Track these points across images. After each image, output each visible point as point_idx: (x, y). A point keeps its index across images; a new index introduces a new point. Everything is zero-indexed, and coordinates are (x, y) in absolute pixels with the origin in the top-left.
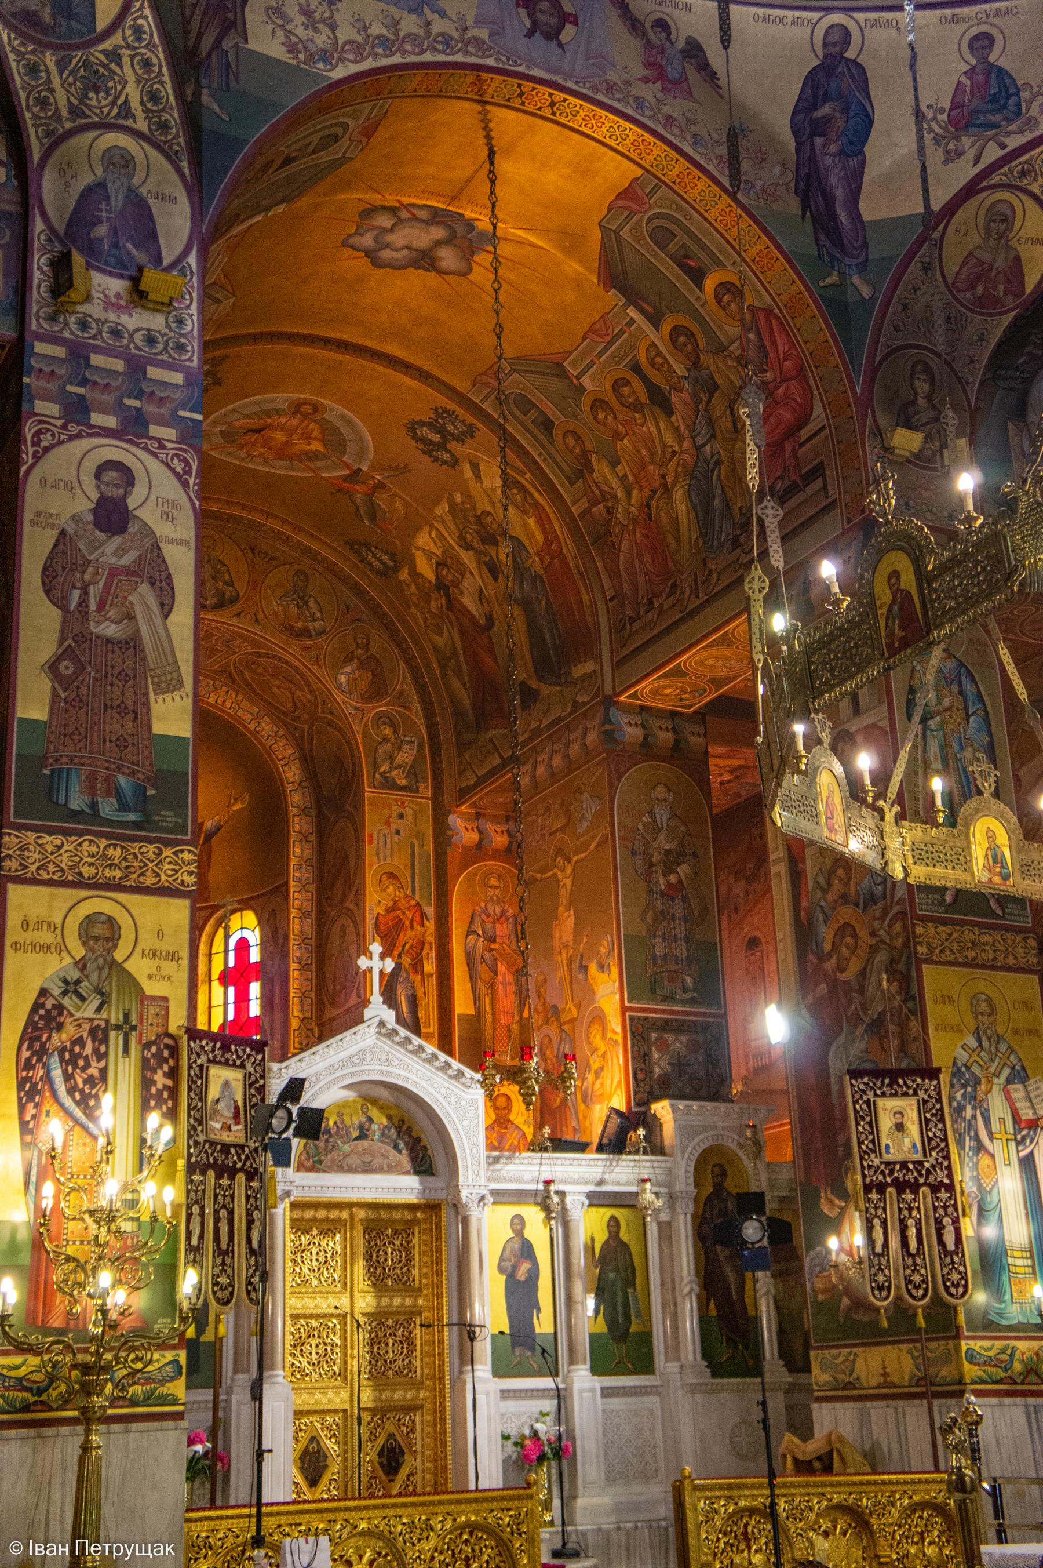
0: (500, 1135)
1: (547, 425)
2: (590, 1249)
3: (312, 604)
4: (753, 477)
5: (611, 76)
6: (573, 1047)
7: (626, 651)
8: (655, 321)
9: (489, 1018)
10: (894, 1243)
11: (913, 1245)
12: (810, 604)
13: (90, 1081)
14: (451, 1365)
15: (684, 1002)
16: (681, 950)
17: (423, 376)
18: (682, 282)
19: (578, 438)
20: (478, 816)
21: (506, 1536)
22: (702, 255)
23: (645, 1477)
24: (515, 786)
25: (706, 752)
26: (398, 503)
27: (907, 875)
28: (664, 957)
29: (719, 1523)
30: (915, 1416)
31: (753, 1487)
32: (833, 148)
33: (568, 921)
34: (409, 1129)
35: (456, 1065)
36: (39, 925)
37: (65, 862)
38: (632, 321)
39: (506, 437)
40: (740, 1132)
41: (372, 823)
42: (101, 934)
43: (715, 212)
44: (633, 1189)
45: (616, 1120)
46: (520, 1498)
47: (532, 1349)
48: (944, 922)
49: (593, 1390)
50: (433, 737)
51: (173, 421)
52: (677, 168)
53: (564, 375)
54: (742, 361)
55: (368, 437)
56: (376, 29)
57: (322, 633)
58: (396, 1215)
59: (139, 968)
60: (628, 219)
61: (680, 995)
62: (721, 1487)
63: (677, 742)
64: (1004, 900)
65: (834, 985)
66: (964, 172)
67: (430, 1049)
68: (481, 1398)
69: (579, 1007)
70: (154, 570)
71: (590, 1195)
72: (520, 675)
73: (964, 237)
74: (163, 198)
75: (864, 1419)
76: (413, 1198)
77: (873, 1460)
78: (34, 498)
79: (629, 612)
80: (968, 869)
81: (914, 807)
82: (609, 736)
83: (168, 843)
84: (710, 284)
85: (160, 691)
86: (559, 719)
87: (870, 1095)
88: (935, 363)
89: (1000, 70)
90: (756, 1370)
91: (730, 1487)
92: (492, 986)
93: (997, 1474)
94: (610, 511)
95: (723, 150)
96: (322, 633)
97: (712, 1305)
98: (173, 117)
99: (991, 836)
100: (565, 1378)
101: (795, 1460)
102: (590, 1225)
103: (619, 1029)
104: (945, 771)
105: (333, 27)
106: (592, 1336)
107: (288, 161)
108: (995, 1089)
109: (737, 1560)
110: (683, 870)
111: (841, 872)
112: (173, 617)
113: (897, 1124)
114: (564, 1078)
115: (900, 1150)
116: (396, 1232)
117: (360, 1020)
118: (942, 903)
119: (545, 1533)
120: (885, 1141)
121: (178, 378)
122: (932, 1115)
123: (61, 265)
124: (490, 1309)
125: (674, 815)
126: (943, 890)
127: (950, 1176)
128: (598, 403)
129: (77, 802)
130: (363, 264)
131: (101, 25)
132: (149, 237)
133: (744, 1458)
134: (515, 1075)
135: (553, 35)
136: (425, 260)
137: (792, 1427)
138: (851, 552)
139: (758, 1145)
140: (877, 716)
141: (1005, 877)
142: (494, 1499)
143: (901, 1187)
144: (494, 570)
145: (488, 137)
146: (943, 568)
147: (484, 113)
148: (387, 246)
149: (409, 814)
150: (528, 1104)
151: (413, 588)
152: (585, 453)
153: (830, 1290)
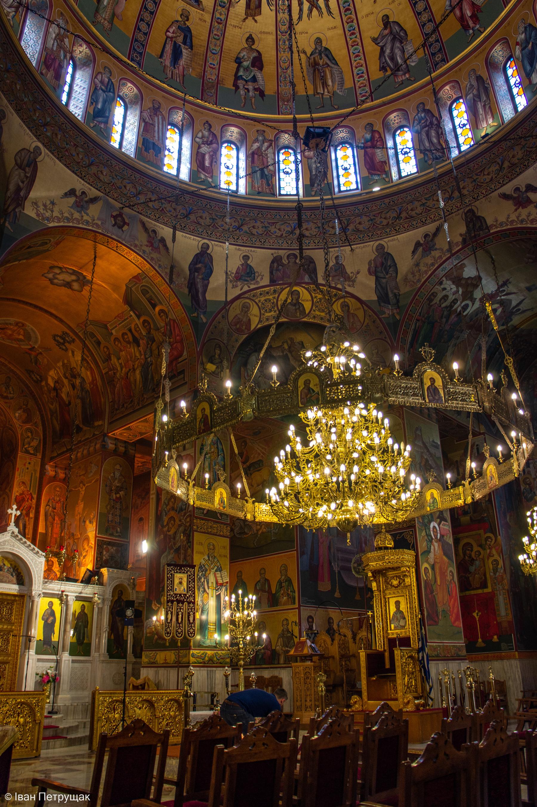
0: (49, 575)
1: (99, 343)
2: (74, 614)
3: (11, 388)
4: (163, 371)
5: (136, 242)
6: (77, 547)
7: (114, 419)
8: (139, 317)
9: (50, 535)
10: (174, 619)
11: (180, 620)
12: (175, 414)
14: (21, 649)
15: (116, 536)
16: (117, 519)
17: (61, 321)
18: (149, 307)
19: (108, 348)
20: (56, 467)
21: (33, 707)
22: (156, 300)
23: (83, 689)
24: (71, 459)
25: (134, 456)
26: (45, 360)
27: (194, 504)
28: (112, 521)
29: (106, 705)
30: (173, 673)
31: (119, 693)
32: (200, 277)
33: (81, 506)
34: (18, 569)
35: (37, 549)
38: (131, 316)
39: (85, 345)
40: (129, 580)
41: (19, 463)
43: (162, 288)
44: (91, 596)
45: (88, 573)
46: (40, 694)
47: (50, 646)
48: (203, 519)
49: (69, 660)
50: (45, 439)
52: (152, 273)
54: (164, 334)
55: (39, 337)
57: (12, 398)
58: (9, 598)
60: (134, 285)
61: (115, 534)
62: (108, 693)
63: (126, 451)
64: (221, 514)
65: (166, 536)
66: (237, 292)
67: (29, 543)
68: (30, 661)
69: (81, 534)
71: (76, 597)
72: (77, 422)
73: (234, 311)
75: (157, 673)
76: (15, 593)
77: (158, 686)
79: (116, 406)
80: (213, 504)
81: (199, 483)
82: (104, 446)
84: (157, 309)
86: (88, 438)
87: (173, 572)
88: (222, 345)
89: (250, 266)
90: (125, 657)
91: (111, 693)
92: (52, 524)
93: (196, 690)
95: (168, 271)
96: (12, 398)
97: (112, 636)
99: (221, 494)
100: (60, 656)
101: (133, 685)
102: (75, 606)
103: (93, 543)
104: (209, 472)
105: (52, 211)
107: (30, 247)
108: (212, 573)
109: (110, 716)
110: (122, 493)
111: (173, 500)
113: (180, 582)
114: (73, 557)
115: (180, 590)
116: (8, 603)
117: (5, 530)
118: (203, 513)
119: (47, 706)
120: (175, 587)
122: (191, 580)
124: (37, 631)
125: (121, 475)
126: (204, 509)
127: (194, 599)
128: (116, 339)
130: (47, 283)
133: (116, 684)
134: (57, 555)
135: (121, 227)
136: (68, 285)
137: (133, 675)
138: (189, 399)
139: (134, 585)
140: (191, 451)
141: (224, 508)
142: (31, 694)
143: (178, 602)
144: (74, 386)
145: (95, 252)
146: (219, 410)
147: (95, 245)
148: (57, 279)
149: (32, 463)
150: (60, 565)
151: (46, 388)
152: (109, 354)
153: (152, 633)
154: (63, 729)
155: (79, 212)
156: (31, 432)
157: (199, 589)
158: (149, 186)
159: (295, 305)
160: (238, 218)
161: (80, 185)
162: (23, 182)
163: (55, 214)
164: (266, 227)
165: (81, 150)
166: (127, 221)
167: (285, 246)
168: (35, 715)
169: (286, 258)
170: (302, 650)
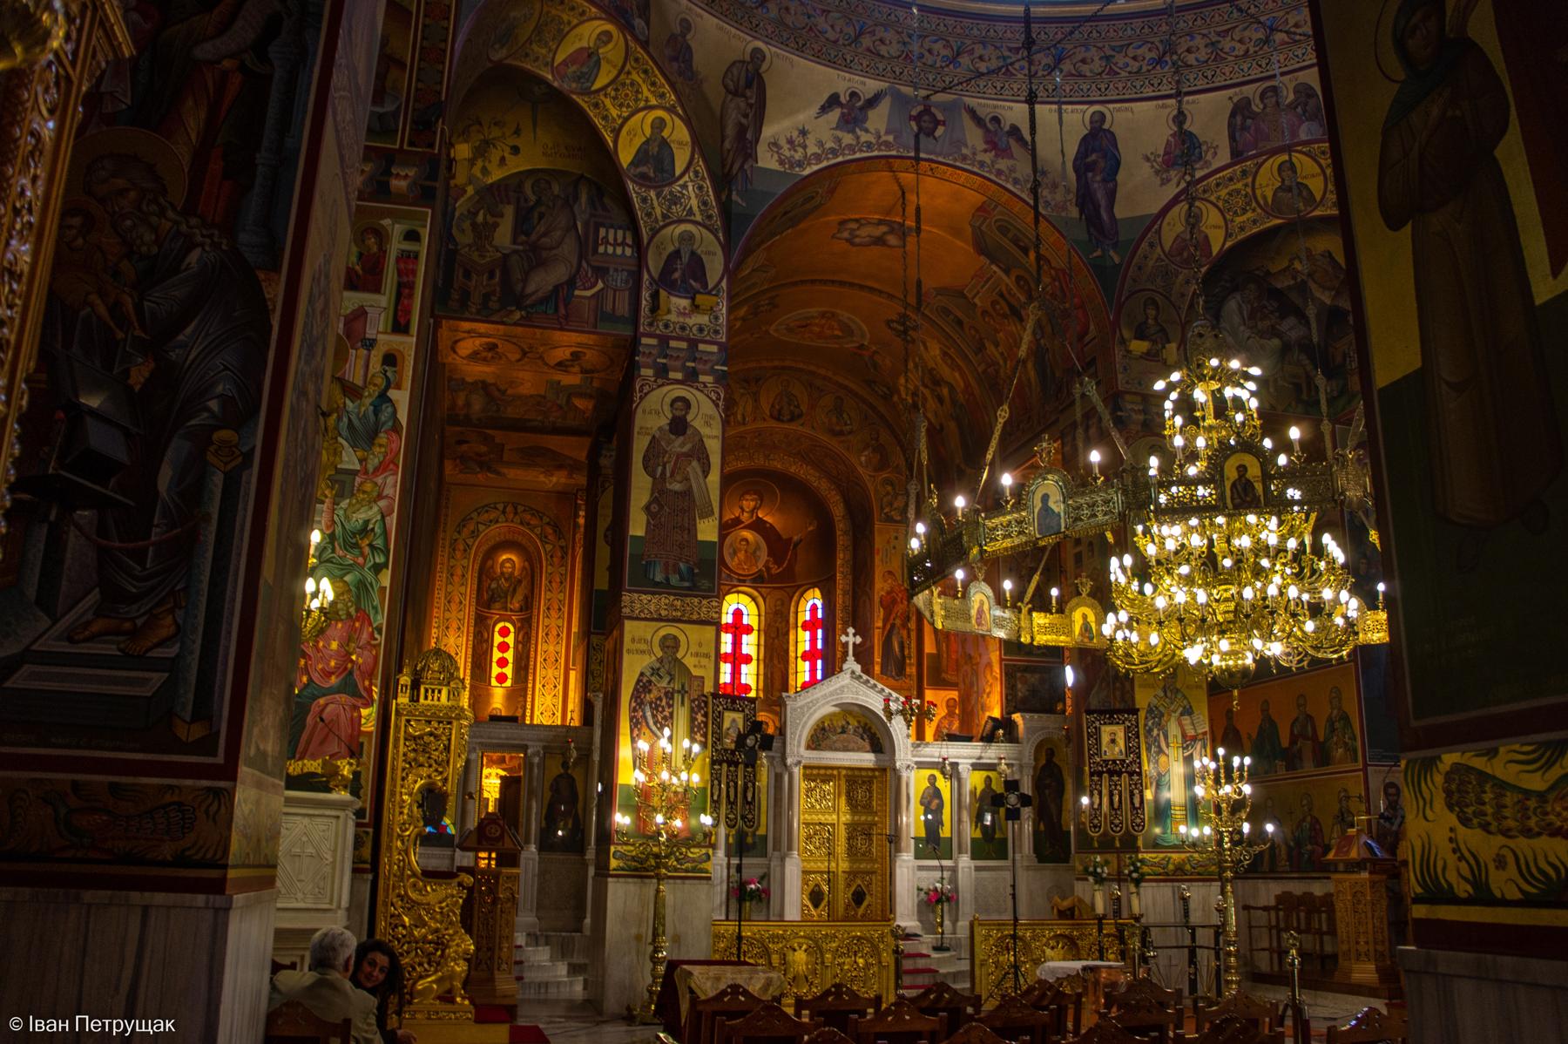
1: (960, 323)
2: (973, 793)
5: (964, 151)
8: (1007, 272)
13: (665, 718)
36: (640, 641)
37: (652, 608)
42: (670, 644)
51: (712, 372)
53: (965, 297)
56: (830, 145)
57: (850, 432)
59: (689, 661)
70: (700, 454)
74: (708, 253)
76: (871, 765)
78: (640, 420)
83: (704, 597)
85: (702, 517)
88: (1158, 298)
94: (997, 372)
96: (850, 432)
98: (715, 212)
102: (974, 781)
106: (973, 840)
112: (710, 478)
113: (1112, 739)
120: (1104, 748)
121: (714, 349)
122: (1132, 735)
123: (655, 296)
124: (913, 820)
128: (984, 313)
129: (659, 578)
131: (678, 173)
132: (702, 279)
143: (1111, 773)
144: (940, 400)
154: (946, 975)
155: (853, 132)
156: (892, 485)
157: (1148, 750)
158: (975, 32)
159: (1290, 189)
160: (1156, 40)
161: (841, 82)
162: (746, 116)
163: (810, 151)
164: (1213, 44)
165: (837, 15)
166: (940, 117)
167: (1256, 73)
168: (879, 955)
169: (1258, 101)
170: (1348, 852)
